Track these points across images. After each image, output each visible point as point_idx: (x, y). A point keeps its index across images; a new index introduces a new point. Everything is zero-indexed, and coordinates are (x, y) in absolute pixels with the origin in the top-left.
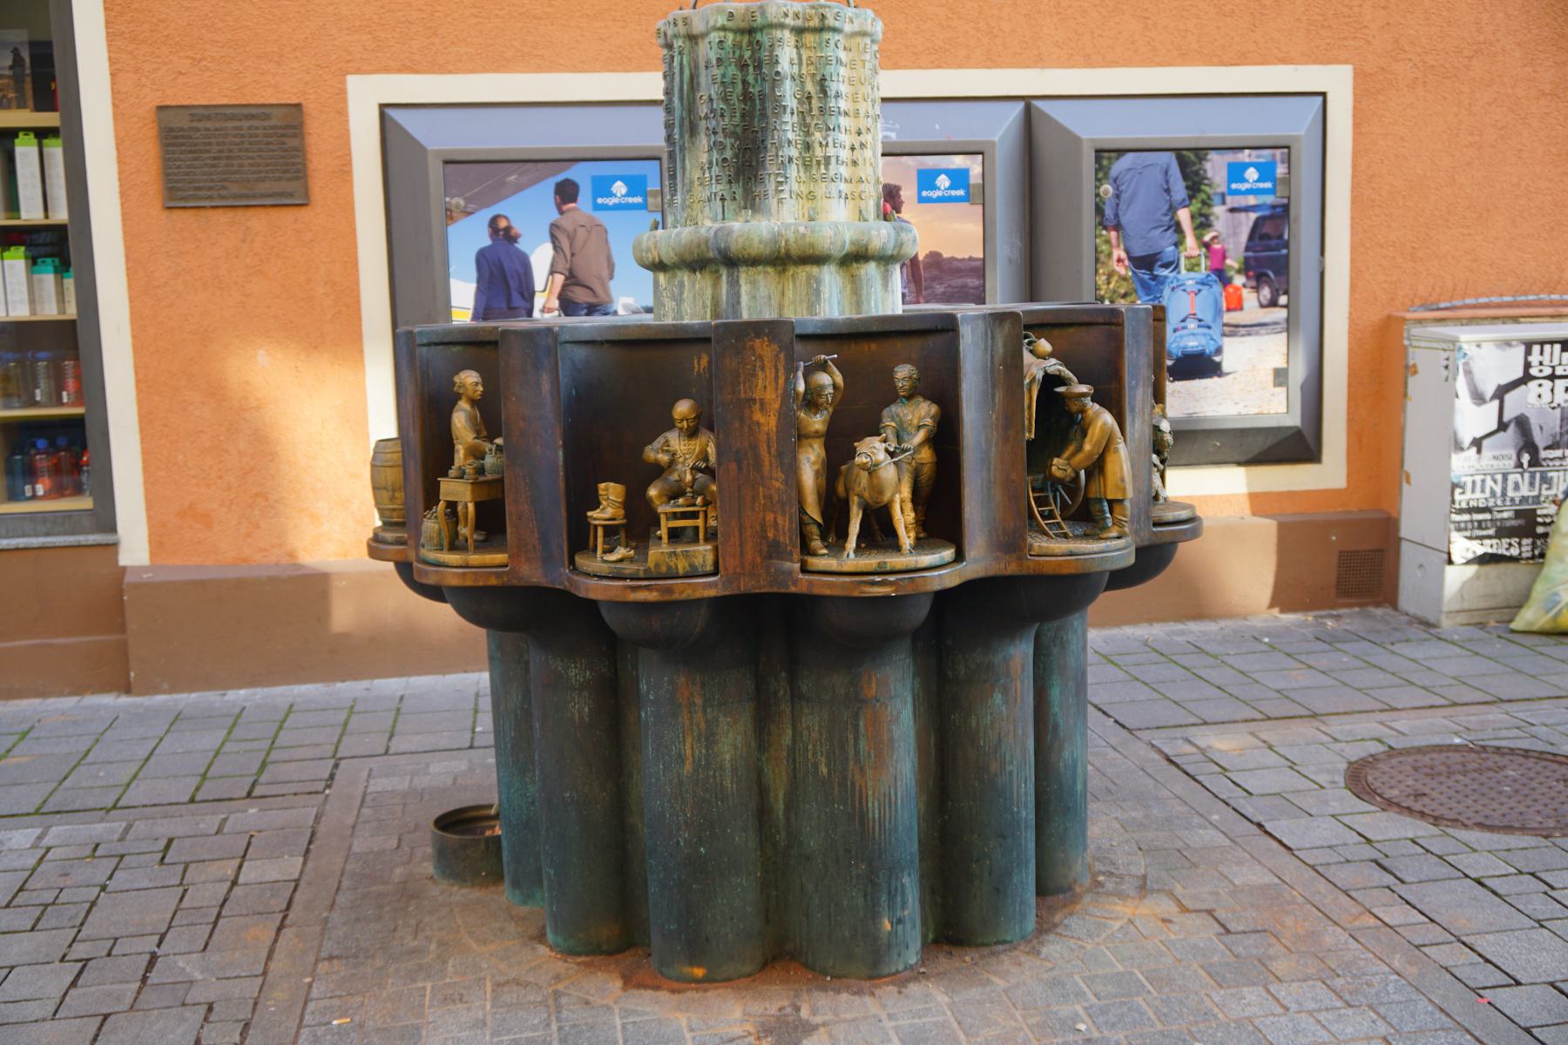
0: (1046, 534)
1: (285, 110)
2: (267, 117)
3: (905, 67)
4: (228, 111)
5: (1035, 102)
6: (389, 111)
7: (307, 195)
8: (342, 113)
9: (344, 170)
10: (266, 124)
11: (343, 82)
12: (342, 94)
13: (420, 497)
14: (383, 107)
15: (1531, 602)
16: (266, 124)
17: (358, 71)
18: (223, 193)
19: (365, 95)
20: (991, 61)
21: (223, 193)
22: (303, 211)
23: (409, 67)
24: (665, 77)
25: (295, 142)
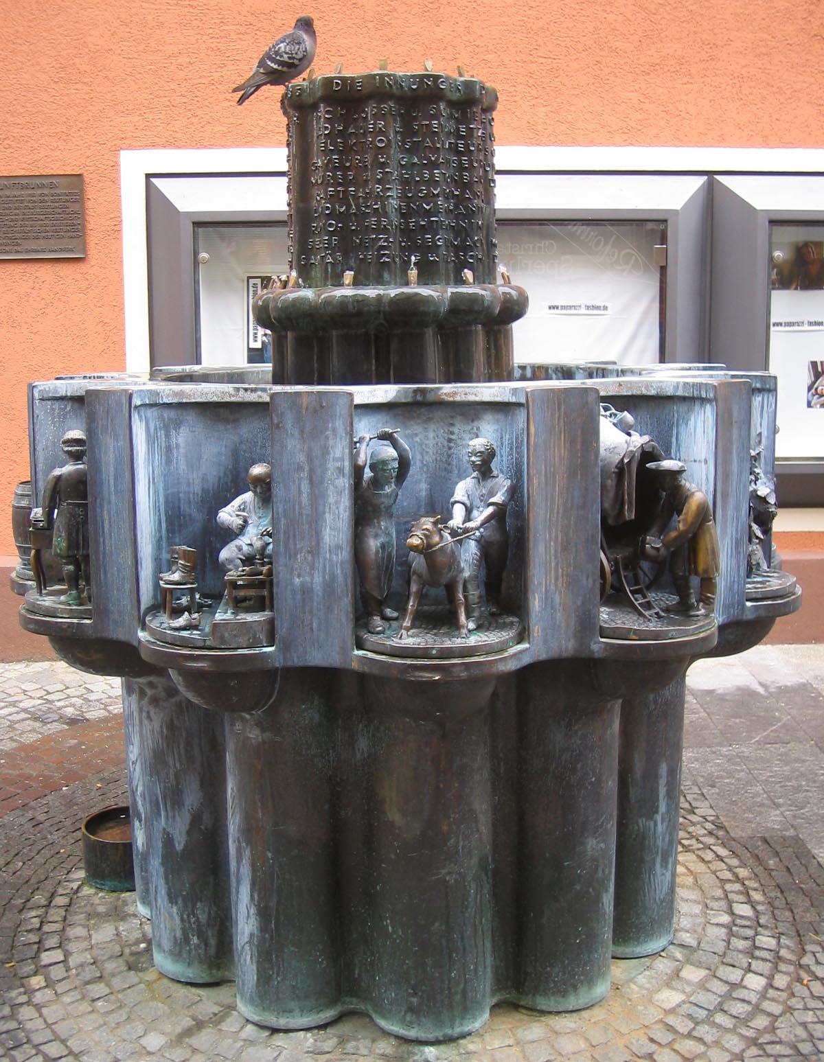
0: (641, 614)
1: (68, 179)
2: (52, 186)
3: (601, 144)
4: (24, 181)
5: (718, 177)
6: (153, 180)
7: (84, 249)
8: (115, 182)
9: (115, 230)
10: (52, 191)
11: (117, 156)
12: (116, 166)
13: (196, 220)
14: (149, 176)
15: (140, 974)
16: (52, 191)
17: (130, 147)
18: (19, 249)
19: (134, 166)
20: (679, 140)
21: (19, 249)
22: (81, 267)
23: (172, 143)
24: (202, 785)
25: (76, 207)
